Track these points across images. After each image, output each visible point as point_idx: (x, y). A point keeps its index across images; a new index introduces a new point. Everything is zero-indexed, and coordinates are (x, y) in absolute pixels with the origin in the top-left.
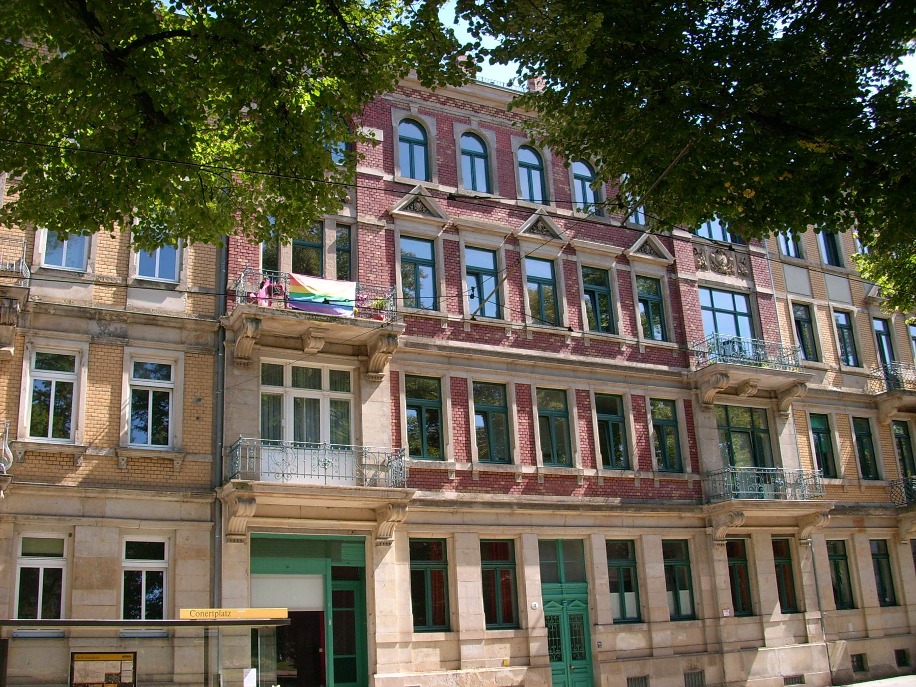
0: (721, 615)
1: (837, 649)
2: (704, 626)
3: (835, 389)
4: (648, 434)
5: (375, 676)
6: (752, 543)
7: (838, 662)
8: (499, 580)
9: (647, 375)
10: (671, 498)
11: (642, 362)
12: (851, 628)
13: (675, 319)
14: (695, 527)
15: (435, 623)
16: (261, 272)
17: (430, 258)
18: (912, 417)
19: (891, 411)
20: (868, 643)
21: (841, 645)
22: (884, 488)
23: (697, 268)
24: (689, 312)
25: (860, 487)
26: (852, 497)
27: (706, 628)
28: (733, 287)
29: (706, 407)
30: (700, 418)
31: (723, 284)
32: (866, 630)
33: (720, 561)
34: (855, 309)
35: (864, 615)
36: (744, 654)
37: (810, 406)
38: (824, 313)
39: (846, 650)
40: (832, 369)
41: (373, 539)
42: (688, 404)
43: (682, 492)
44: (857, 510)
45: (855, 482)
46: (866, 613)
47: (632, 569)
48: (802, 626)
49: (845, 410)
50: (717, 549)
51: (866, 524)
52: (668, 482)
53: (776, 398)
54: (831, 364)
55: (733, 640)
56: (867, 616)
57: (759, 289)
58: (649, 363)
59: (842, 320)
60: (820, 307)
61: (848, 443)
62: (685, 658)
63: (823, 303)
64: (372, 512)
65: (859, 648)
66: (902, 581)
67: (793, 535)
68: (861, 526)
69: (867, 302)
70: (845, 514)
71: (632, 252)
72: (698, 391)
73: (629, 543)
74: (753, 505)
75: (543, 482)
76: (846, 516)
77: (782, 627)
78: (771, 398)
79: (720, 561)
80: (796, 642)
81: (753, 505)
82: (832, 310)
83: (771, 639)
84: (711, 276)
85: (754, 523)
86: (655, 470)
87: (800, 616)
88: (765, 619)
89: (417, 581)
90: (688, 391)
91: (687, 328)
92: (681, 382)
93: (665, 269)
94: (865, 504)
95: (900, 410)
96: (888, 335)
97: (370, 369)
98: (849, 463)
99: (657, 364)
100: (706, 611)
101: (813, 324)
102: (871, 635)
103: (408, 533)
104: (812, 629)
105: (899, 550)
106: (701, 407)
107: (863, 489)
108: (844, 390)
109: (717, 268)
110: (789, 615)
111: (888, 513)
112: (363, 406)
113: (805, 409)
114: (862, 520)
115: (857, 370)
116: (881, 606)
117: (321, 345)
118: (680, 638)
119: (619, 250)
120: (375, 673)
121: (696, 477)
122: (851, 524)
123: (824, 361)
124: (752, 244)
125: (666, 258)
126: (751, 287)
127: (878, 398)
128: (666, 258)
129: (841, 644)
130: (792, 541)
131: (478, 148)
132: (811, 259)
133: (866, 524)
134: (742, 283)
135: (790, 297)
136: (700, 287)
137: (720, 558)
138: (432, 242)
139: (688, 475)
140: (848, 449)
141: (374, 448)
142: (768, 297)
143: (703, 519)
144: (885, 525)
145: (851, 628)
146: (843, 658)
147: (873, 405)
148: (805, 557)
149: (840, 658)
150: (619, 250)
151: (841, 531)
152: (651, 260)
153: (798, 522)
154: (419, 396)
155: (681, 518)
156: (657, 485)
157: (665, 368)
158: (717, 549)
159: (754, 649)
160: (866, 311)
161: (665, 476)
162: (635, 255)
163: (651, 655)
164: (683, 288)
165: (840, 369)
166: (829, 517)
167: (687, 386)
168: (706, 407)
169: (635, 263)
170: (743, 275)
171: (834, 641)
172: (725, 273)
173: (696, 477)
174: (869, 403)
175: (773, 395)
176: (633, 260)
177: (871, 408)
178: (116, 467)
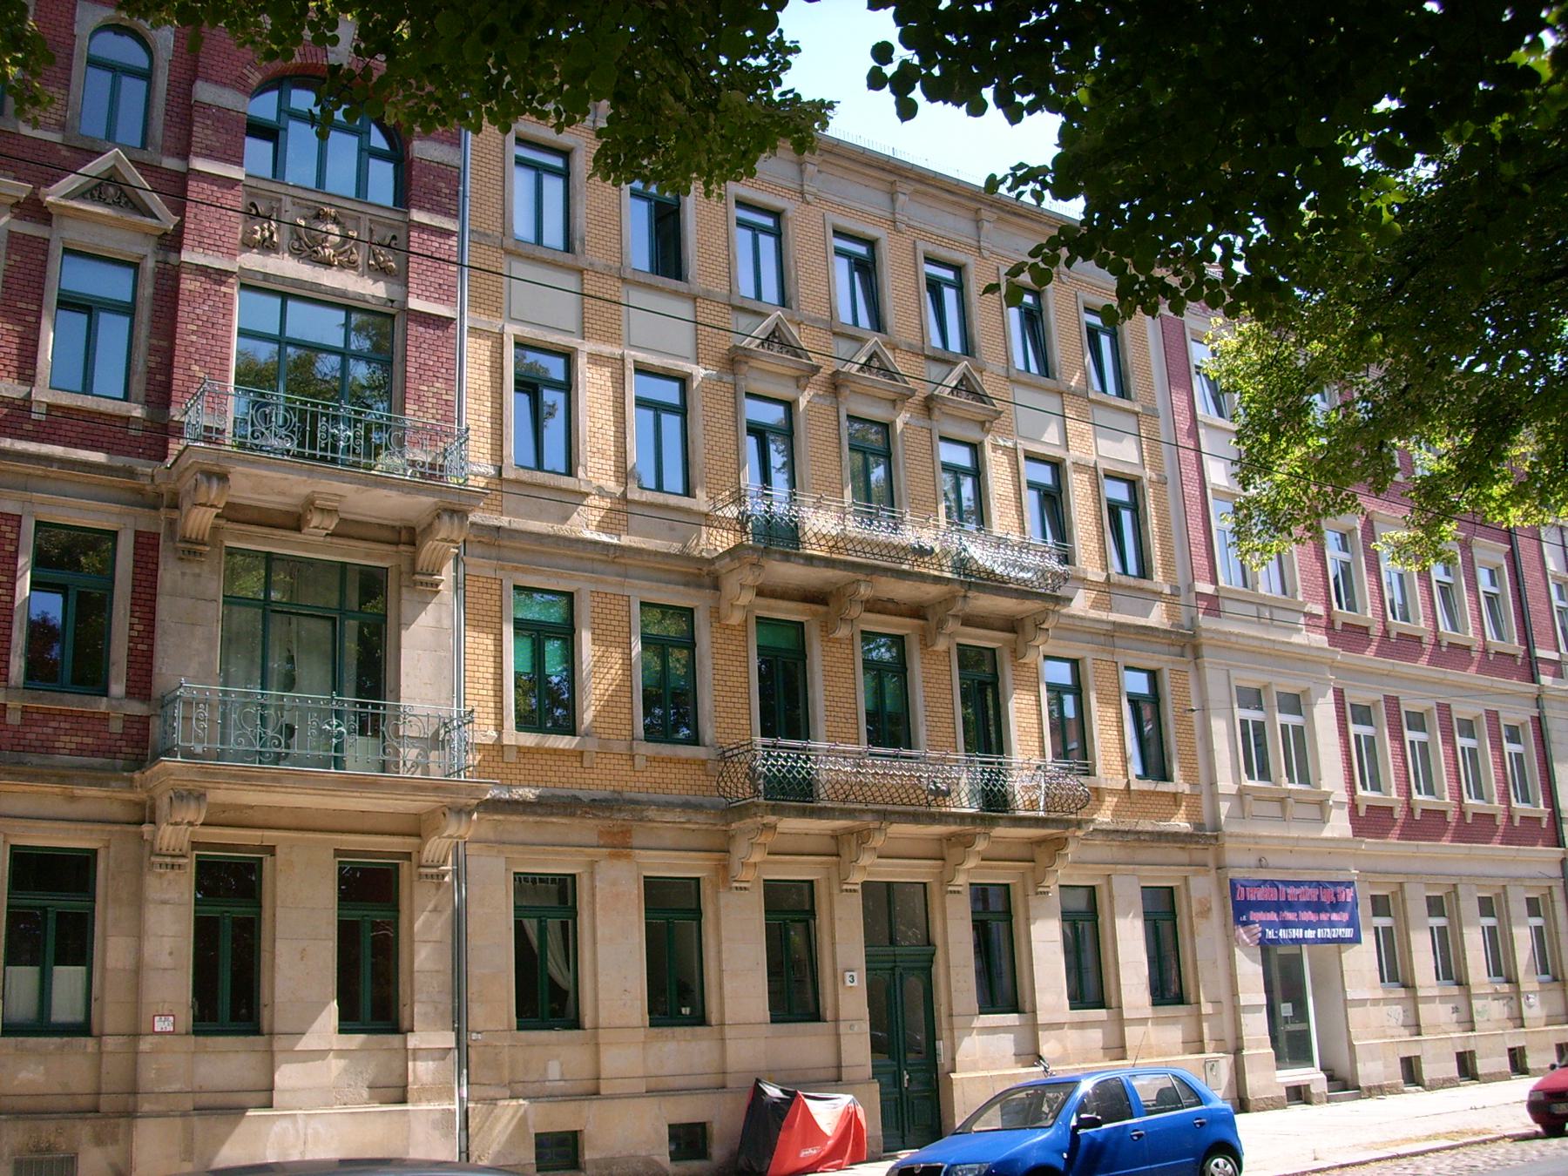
0: (145, 1028)
1: (497, 1119)
2: (100, 1053)
3: (604, 538)
4: (13, 602)
5: (953, 1075)
6: (274, 865)
7: (495, 1148)
8: (367, 937)
9: (38, 470)
10: (49, 750)
11: (33, 439)
12: (554, 1071)
13: (153, 350)
14: (699, 851)
15: (235, 1017)
16: (231, 390)
17: (129, 300)
18: (815, 614)
19: (741, 599)
20: (591, 1109)
21: (510, 1111)
22: (704, 763)
23: (248, 245)
24: (194, 338)
25: (632, 757)
26: (597, 781)
27: (105, 1058)
28: (343, 294)
29: (191, 550)
30: (170, 574)
31: (316, 286)
32: (839, 1067)
33: (164, 902)
34: (699, 372)
35: (723, 1039)
36: (197, 1122)
37: (516, 569)
38: (607, 371)
39: (523, 1121)
40: (602, 493)
41: (414, 866)
42: (147, 546)
43: (86, 740)
44: (611, 808)
45: (621, 747)
46: (601, 1041)
47: (570, 922)
48: (396, 1064)
49: (622, 585)
50: (161, 875)
51: (635, 842)
52: (49, 715)
53: (413, 544)
54: (602, 483)
55: (176, 1087)
56: (602, 1048)
57: (415, 304)
58: (54, 443)
59: (1044, 475)
60: (595, 359)
61: (616, 657)
62: (21, 1125)
63: (607, 349)
64: (833, 842)
65: (561, 1119)
66: (721, 971)
67: (408, 856)
68: (619, 845)
69: (734, 361)
70: (573, 815)
71: (53, 196)
72: (175, 514)
73: (569, 879)
74: (235, 776)
75: (514, 760)
76: (577, 821)
77: (336, 1065)
78: (397, 543)
79: (164, 902)
80: (372, 1099)
81: (235, 776)
82: (630, 366)
83: (294, 1090)
84: (286, 266)
85: (285, 821)
86: (12, 683)
87: (394, 1040)
88: (279, 1043)
89: (205, 931)
90: (153, 513)
91: (178, 374)
92: (140, 491)
93: (153, 242)
94: (643, 797)
95: (761, 593)
96: (1136, 506)
97: (419, 569)
98: (609, 705)
99: (76, 446)
100: (111, 1016)
101: (573, 392)
102: (605, 1089)
103: (5, 835)
104: (422, 1071)
105: (722, 903)
106: (176, 549)
107: (640, 762)
108: (626, 540)
109: (308, 250)
110: (361, 1037)
111: (701, 818)
112: (403, 632)
113: (500, 574)
114: (626, 833)
115: (685, 502)
116: (774, 1020)
117: (332, 524)
118: (24, 1075)
119: (22, 189)
120: (954, 1071)
121: (137, 708)
122: (594, 839)
123: (581, 474)
124: (198, 155)
125: (154, 216)
126: (397, 297)
127: (717, 565)
128: (154, 216)
129: (510, 1111)
130: (405, 867)
131: (139, 59)
132: (593, 253)
133: (635, 842)
134: (374, 289)
135: (512, 330)
136: (244, 286)
137: (167, 897)
138: (135, 266)
139: (117, 700)
140: (615, 669)
141: (421, 708)
142: (443, 323)
143: (140, 805)
144: (920, 853)
145: (554, 1071)
146: (511, 1140)
147: (707, 580)
148: (430, 907)
149: (504, 1138)
150: (22, 189)
151: (558, 853)
152: (111, 218)
153: (417, 828)
154: (58, 565)
155: (73, 798)
156: (14, 718)
157: (99, 457)
158: (161, 875)
159: (236, 1111)
160: (728, 378)
161: (34, 699)
162: (63, 202)
163: (597, 1093)
164: (189, 284)
165: (624, 494)
166: (475, 816)
167: (153, 502)
168: (191, 550)
169: (67, 222)
170: (381, 272)
171: (493, 1101)
172: (327, 264)
173: (137, 708)
174: (699, 576)
175: (404, 536)
176: (62, 215)
177: (700, 586)
178: (499, 759)
